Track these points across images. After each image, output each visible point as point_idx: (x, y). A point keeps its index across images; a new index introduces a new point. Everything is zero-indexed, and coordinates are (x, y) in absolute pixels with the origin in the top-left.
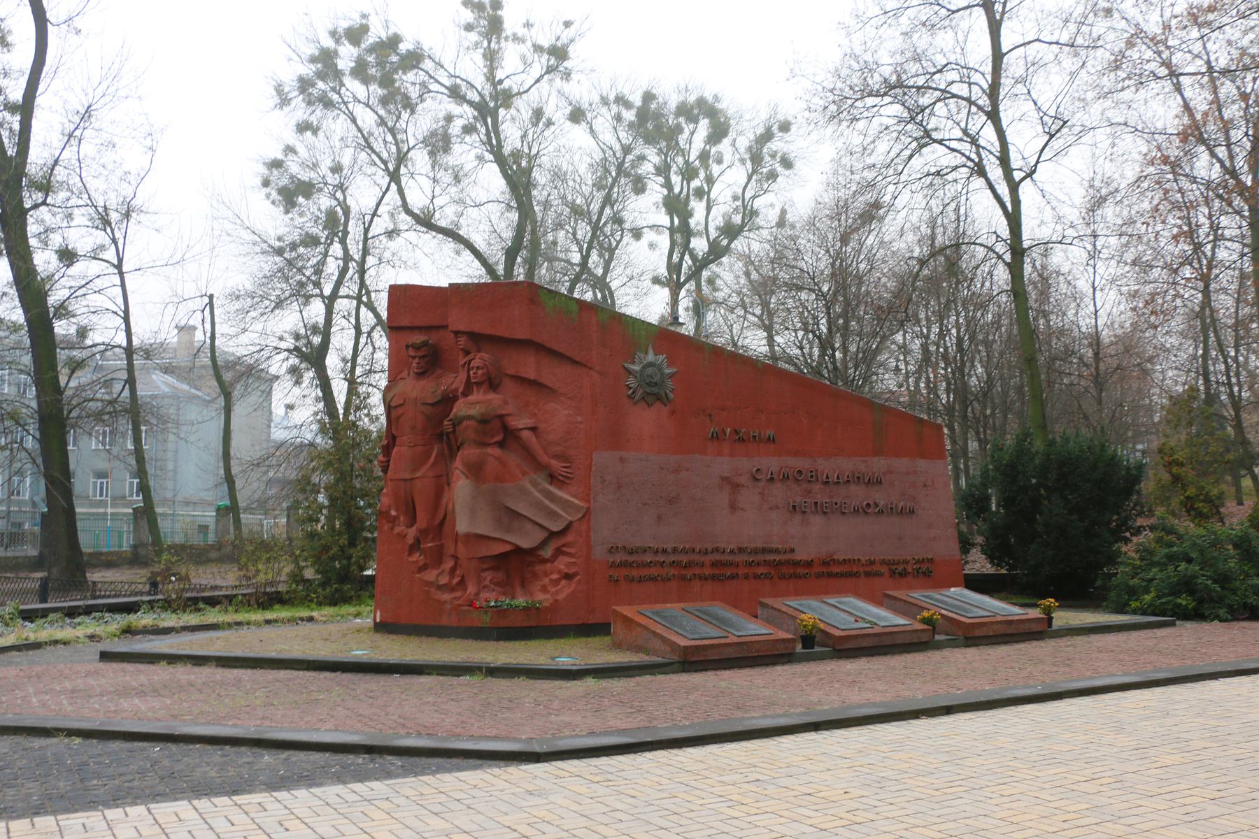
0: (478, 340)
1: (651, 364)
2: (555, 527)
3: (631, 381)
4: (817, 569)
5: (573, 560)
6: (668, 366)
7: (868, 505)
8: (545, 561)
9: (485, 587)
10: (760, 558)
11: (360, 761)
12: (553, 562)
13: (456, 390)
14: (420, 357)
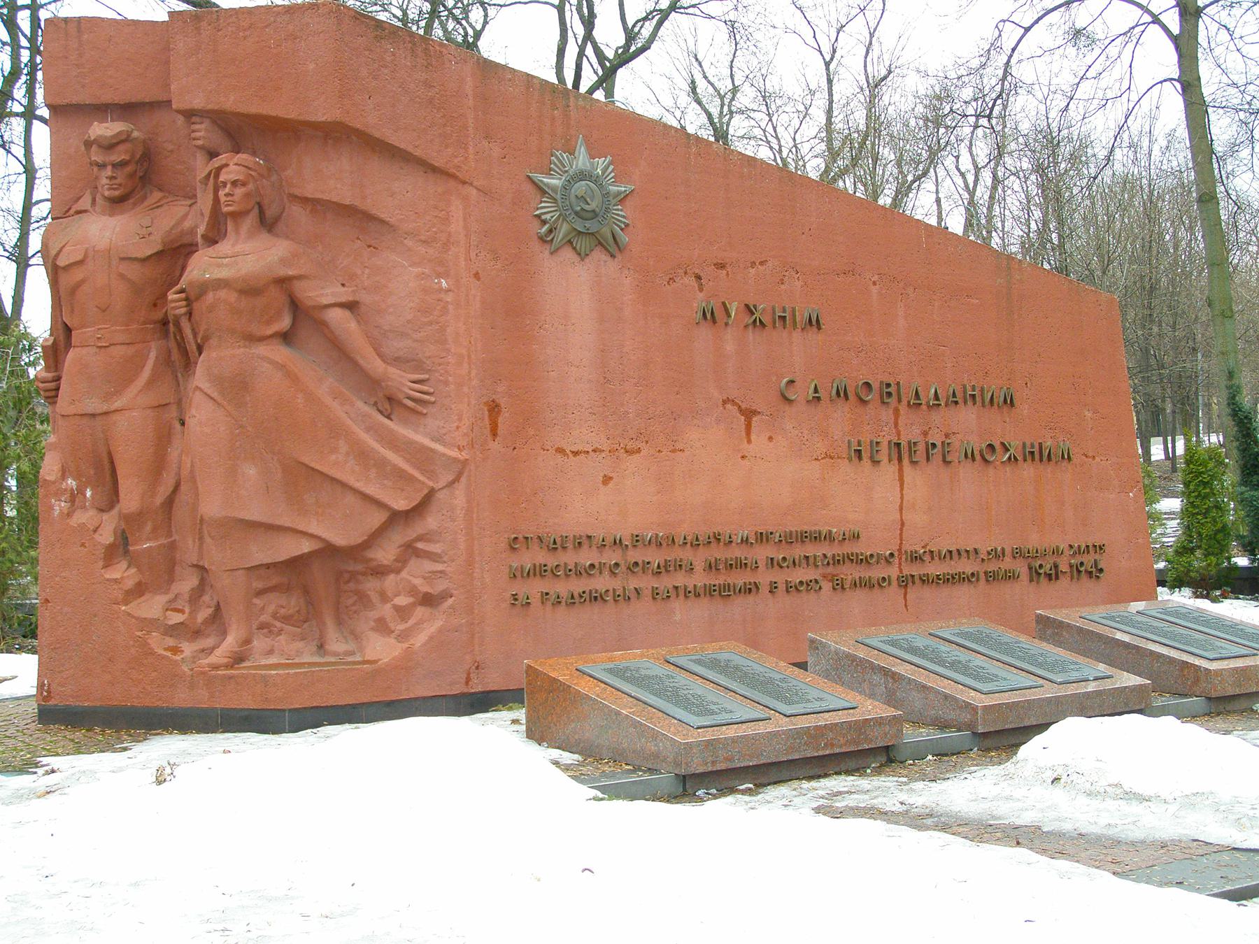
0: (238, 130)
1: (582, 176)
2: (401, 504)
6: (617, 180)
8: (380, 572)
10: (798, 551)
13: (192, 231)
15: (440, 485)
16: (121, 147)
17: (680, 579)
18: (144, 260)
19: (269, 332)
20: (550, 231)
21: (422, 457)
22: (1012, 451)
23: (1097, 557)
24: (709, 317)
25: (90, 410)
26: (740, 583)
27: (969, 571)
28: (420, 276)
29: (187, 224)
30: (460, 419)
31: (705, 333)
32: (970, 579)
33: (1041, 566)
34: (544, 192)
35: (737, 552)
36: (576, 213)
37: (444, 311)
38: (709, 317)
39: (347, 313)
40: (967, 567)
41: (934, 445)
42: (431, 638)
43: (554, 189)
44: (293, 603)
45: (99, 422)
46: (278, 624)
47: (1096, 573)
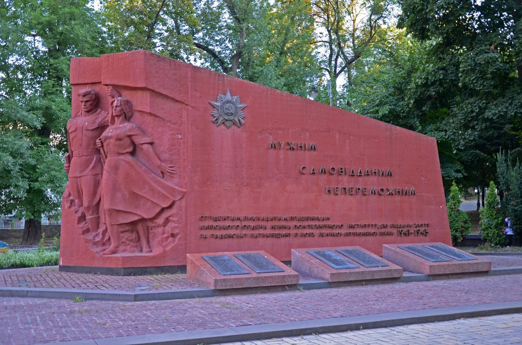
1: (228, 102)
3: (215, 112)
4: (343, 231)
5: (176, 225)
6: (241, 103)
7: (382, 190)
9: (122, 243)
10: (306, 223)
11: (488, 279)
12: (164, 226)
13: (108, 121)
14: (86, 102)
15: (177, 199)
16: (88, 96)
17: (262, 231)
18: (93, 130)
19: (125, 152)
20: (217, 120)
21: (172, 190)
22: (391, 191)
23: (426, 228)
24: (274, 147)
25: (76, 176)
26: (284, 233)
27: (373, 231)
28: (172, 134)
29: (106, 119)
30: (184, 179)
31: (272, 152)
32: (374, 234)
33: (402, 231)
34: (214, 107)
35: (283, 223)
36: (226, 114)
37: (180, 145)
38: (274, 147)
39: (150, 146)
40: (372, 231)
41: (359, 189)
42: (172, 247)
43: (218, 106)
44: (134, 236)
45: (78, 179)
46: (128, 242)
47: (425, 234)
